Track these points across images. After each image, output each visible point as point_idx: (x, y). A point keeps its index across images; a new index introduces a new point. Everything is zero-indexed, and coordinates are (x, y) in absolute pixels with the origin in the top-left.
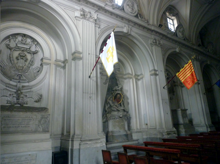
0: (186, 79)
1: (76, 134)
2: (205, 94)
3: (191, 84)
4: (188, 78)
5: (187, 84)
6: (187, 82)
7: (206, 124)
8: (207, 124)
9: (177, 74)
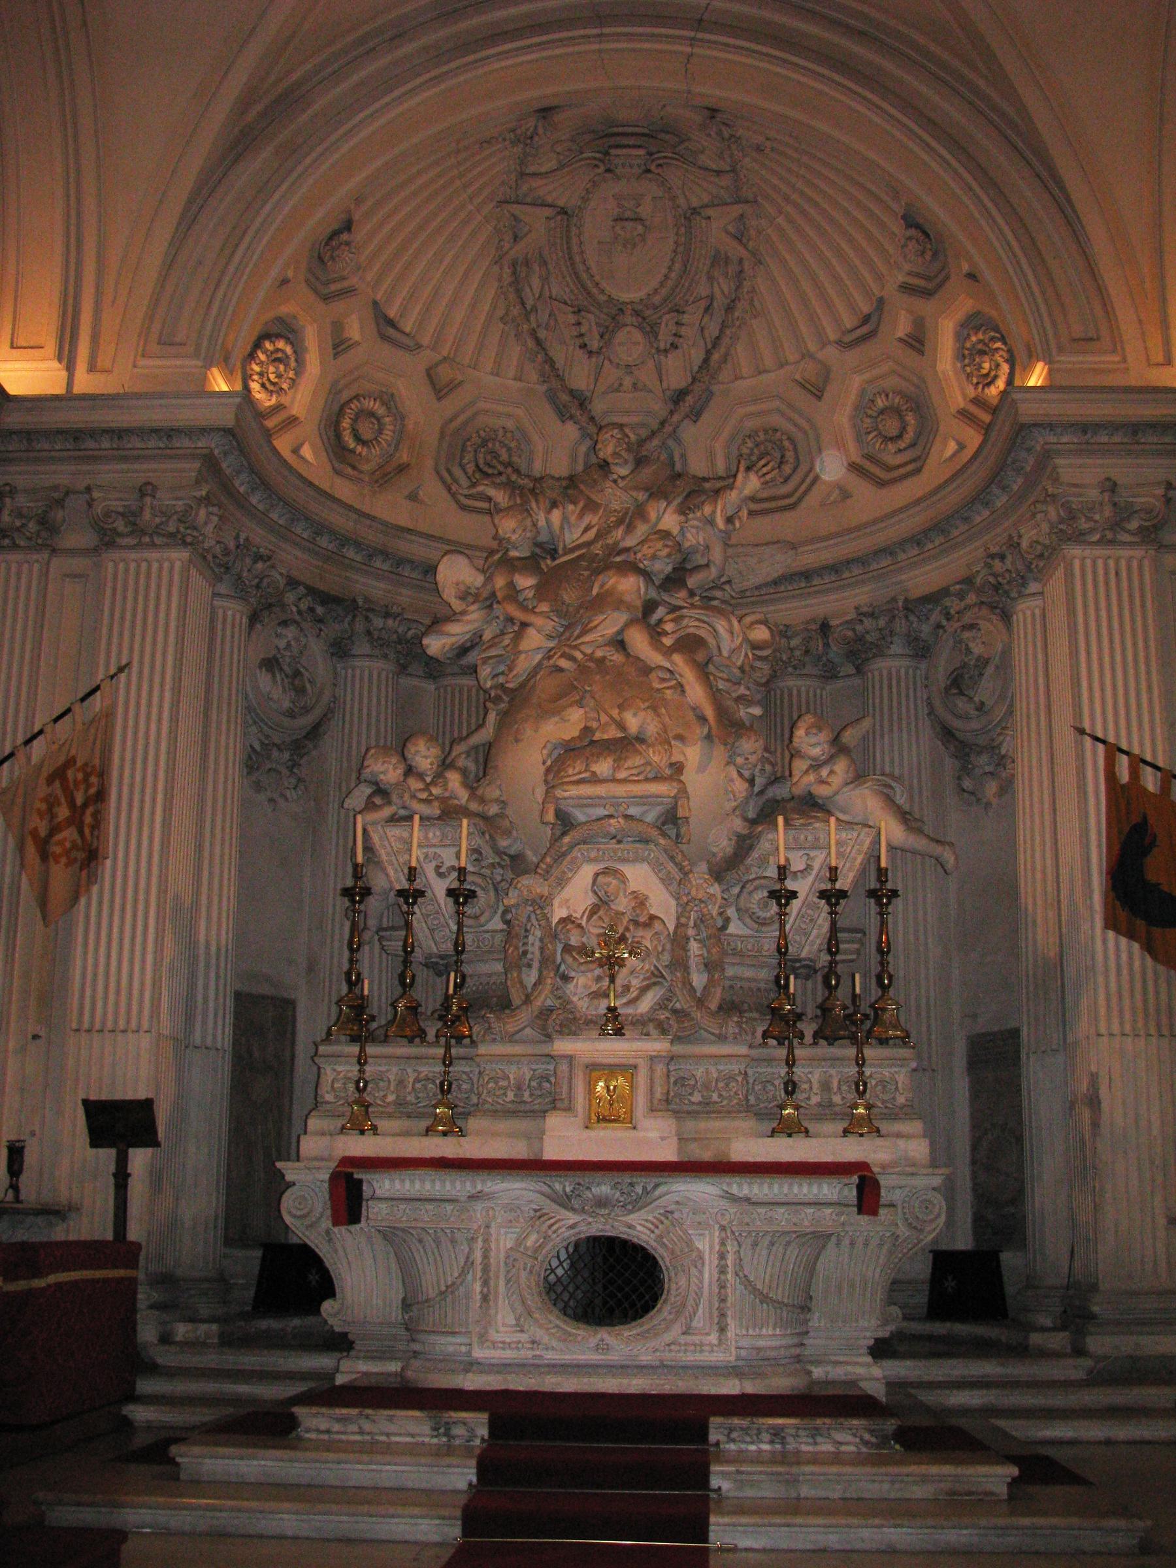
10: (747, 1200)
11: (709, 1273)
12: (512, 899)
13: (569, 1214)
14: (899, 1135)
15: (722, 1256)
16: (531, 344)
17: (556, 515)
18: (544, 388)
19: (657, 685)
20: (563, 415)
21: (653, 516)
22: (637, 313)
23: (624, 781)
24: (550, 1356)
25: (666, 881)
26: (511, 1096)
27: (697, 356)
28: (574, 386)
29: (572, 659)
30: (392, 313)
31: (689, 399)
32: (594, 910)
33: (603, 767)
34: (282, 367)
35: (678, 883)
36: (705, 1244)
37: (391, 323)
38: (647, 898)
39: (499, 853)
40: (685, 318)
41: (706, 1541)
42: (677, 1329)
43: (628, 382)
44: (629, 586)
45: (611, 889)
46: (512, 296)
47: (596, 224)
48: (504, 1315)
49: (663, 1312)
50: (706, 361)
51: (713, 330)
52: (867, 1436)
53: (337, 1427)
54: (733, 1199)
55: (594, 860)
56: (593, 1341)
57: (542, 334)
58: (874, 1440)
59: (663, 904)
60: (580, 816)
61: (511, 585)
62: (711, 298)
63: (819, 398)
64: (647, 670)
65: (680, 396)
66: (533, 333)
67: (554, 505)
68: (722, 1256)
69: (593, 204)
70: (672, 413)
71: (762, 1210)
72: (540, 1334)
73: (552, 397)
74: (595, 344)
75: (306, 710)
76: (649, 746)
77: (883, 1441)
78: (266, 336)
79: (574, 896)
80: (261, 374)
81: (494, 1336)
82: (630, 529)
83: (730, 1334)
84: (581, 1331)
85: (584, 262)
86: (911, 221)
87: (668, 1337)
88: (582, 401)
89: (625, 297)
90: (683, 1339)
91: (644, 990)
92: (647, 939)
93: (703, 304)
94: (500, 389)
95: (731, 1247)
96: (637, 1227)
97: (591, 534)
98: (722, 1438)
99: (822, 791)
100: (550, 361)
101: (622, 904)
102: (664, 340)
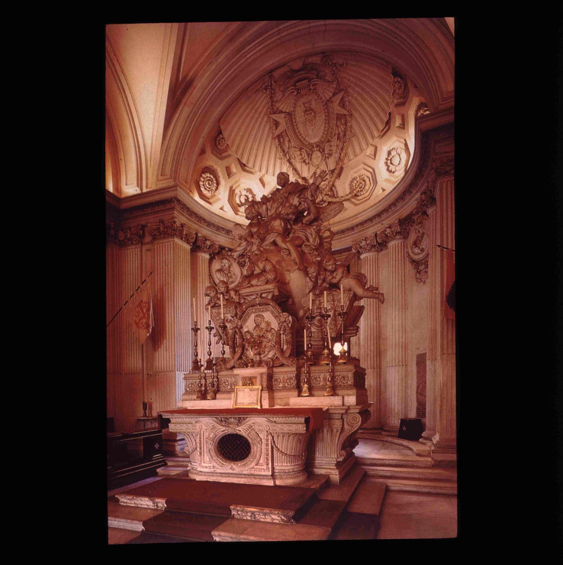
10: (275, 422)
13: (221, 427)
15: (267, 440)
22: (317, 146)
24: (219, 471)
26: (229, 387)
27: (337, 155)
28: (303, 176)
30: (244, 162)
34: (210, 183)
38: (270, 323)
40: (332, 143)
42: (253, 464)
45: (259, 321)
49: (250, 458)
52: (283, 517)
53: (129, 501)
54: (272, 422)
55: (255, 312)
58: (285, 519)
62: (339, 134)
69: (297, 109)
71: (279, 426)
72: (215, 464)
76: (267, 273)
77: (289, 519)
78: (204, 172)
80: (204, 185)
85: (299, 132)
87: (251, 466)
90: (256, 467)
91: (269, 352)
93: (336, 136)
96: (242, 430)
98: (236, 514)
101: (263, 325)
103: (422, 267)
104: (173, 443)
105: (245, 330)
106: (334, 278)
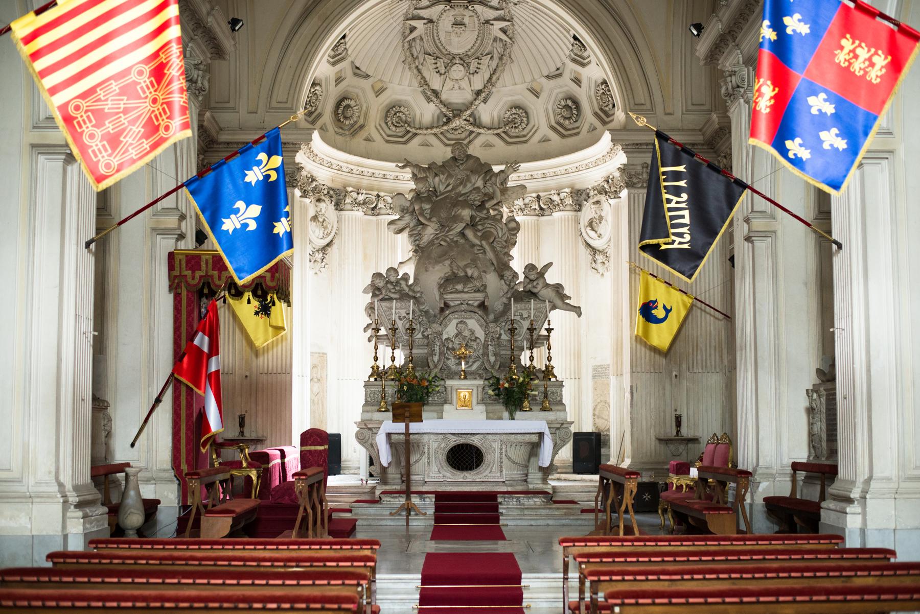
0: (91, 91)
1: (875, 475)
2: (93, 246)
3: (127, 140)
4: (115, 86)
5: (99, 133)
6: (100, 117)
7: (62, 479)
8: (69, 486)
9: (22, 26)
11: (497, 455)
12: (429, 331)
14: (558, 410)
15: (501, 449)
16: (415, 71)
17: (437, 179)
18: (421, 89)
19: (476, 252)
20: (429, 100)
21: (473, 181)
23: (467, 292)
25: (481, 326)
27: (487, 76)
29: (446, 241)
31: (483, 95)
32: (457, 336)
33: (459, 287)
35: (485, 327)
36: (496, 446)
37: (358, 68)
39: (421, 311)
40: (482, 62)
41: (498, 535)
42: (487, 472)
43: (456, 86)
44: (466, 213)
46: (408, 54)
47: (446, 23)
48: (434, 468)
50: (490, 78)
51: (494, 65)
56: (462, 475)
57: (420, 67)
59: (480, 333)
60: (452, 304)
61: (421, 208)
63: (538, 97)
64: (473, 246)
65: (478, 93)
66: (417, 67)
67: (436, 175)
68: (501, 449)
70: (475, 100)
73: (424, 93)
74: (443, 70)
75: (328, 234)
79: (450, 330)
81: (431, 475)
82: (465, 186)
83: (504, 472)
84: (458, 473)
86: (575, 38)
88: (436, 93)
89: (455, 51)
91: (474, 362)
92: (474, 344)
94: (402, 88)
95: (504, 447)
97: (450, 188)
99: (535, 291)
100: (423, 78)
102: (472, 69)
103: (600, 258)
104: (82, 498)
105: (445, 336)
106: (534, 287)
